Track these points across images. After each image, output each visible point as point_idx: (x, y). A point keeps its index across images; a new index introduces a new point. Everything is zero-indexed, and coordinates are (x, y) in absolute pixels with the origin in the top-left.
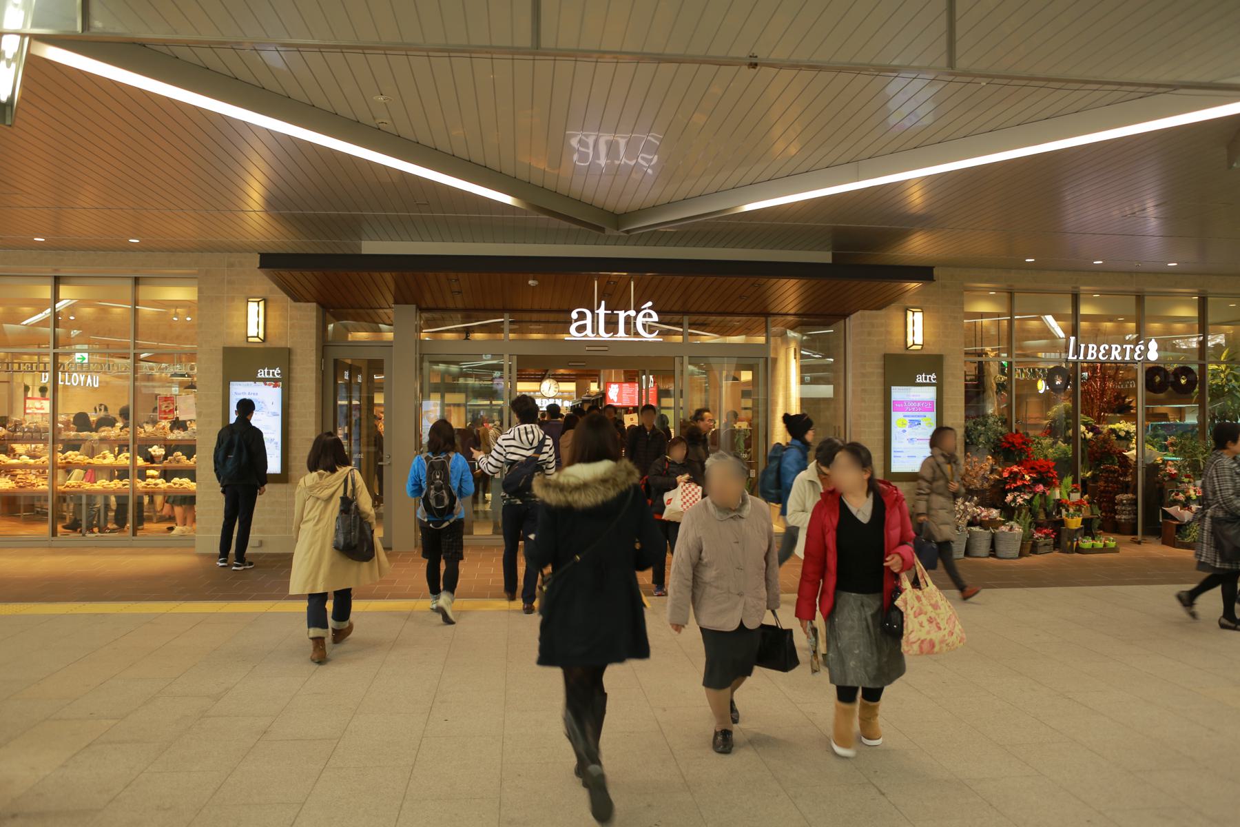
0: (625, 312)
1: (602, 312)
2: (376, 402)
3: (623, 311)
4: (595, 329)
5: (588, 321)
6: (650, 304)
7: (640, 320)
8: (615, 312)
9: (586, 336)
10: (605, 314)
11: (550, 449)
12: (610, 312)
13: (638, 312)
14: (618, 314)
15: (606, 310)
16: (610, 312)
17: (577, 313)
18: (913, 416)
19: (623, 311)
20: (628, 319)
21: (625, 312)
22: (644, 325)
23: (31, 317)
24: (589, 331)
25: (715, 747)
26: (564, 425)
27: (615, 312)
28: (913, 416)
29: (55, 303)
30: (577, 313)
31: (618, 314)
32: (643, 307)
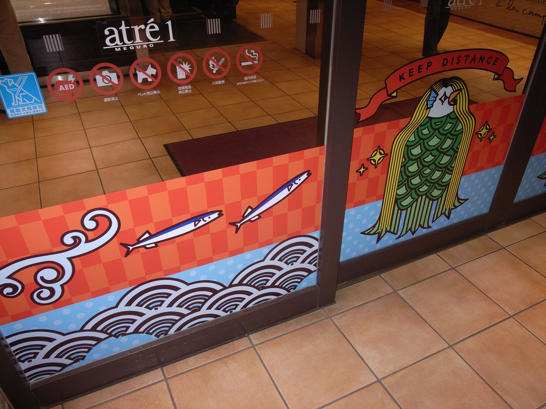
0: (138, 27)
1: (123, 28)
2: (108, 98)
3: (137, 26)
4: (121, 40)
5: (116, 35)
6: (152, 20)
7: (148, 31)
8: (132, 27)
9: (117, 45)
10: (126, 29)
11: (152, 93)
12: (129, 28)
13: (146, 25)
14: (134, 28)
15: (126, 26)
16: (129, 28)
17: (108, 30)
18: (18, 92)
19: (137, 26)
20: (140, 30)
21: (138, 27)
22: (151, 32)
23: (414, 113)
24: (118, 41)
25: (404, 79)
26: (448, 21)
27: (132, 27)
28: (18, 92)
29: (337, 285)
30: (108, 30)
31: (134, 28)
32: (148, 23)
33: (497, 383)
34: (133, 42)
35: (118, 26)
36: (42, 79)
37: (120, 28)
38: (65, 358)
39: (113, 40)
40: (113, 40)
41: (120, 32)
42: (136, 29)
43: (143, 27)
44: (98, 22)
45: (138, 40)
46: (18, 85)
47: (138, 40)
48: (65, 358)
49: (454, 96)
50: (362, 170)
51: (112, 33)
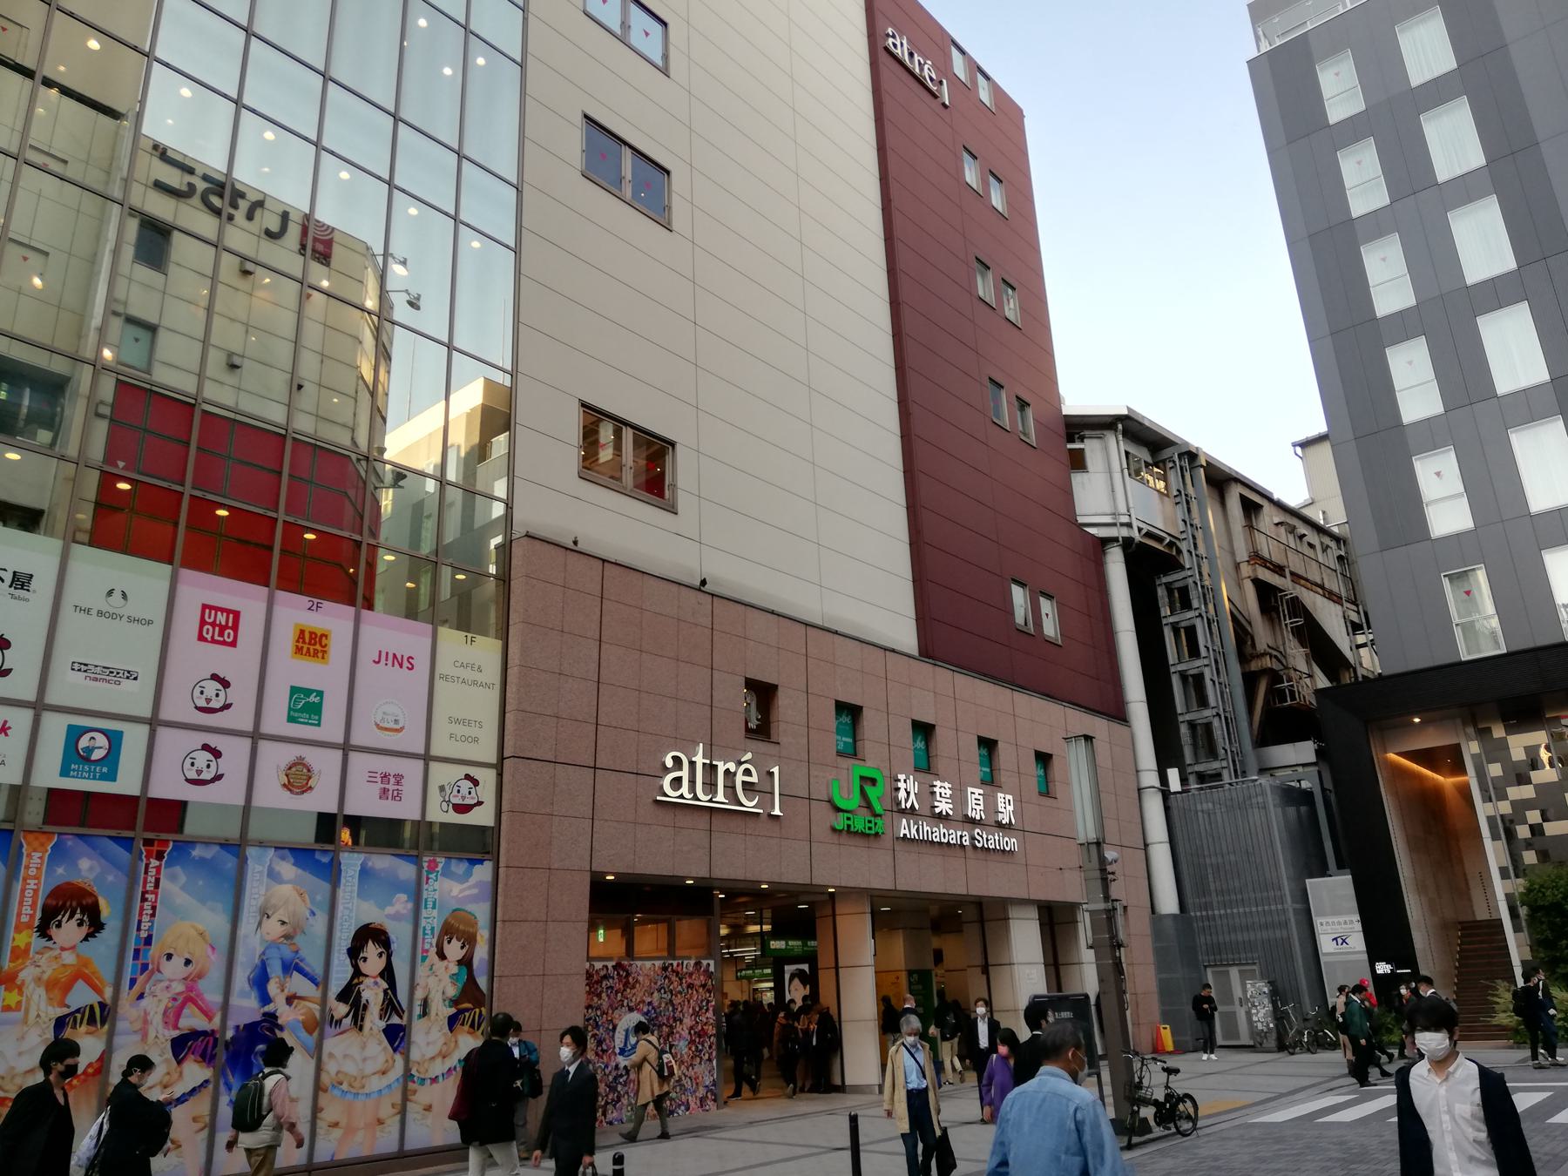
1: (699, 760)
5: (684, 773)
6: (749, 756)
7: (740, 778)
8: (714, 763)
9: (681, 796)
16: (708, 762)
17: (673, 758)
20: (727, 772)
22: (744, 783)
24: (685, 790)
33: (647, 34)
34: (711, 799)
35: (690, 754)
36: (438, 825)
37: (694, 759)
38: (1241, 495)
39: (677, 782)
40: (677, 782)
41: (692, 764)
42: (721, 767)
43: (732, 766)
44: (1070, 1054)
45: (720, 797)
46: (1460, 1035)
47: (720, 797)
48: (1241, 495)
49: (323, 717)
50: (951, 1019)
51: (677, 760)
